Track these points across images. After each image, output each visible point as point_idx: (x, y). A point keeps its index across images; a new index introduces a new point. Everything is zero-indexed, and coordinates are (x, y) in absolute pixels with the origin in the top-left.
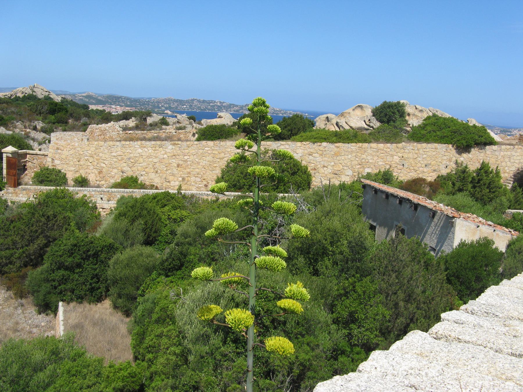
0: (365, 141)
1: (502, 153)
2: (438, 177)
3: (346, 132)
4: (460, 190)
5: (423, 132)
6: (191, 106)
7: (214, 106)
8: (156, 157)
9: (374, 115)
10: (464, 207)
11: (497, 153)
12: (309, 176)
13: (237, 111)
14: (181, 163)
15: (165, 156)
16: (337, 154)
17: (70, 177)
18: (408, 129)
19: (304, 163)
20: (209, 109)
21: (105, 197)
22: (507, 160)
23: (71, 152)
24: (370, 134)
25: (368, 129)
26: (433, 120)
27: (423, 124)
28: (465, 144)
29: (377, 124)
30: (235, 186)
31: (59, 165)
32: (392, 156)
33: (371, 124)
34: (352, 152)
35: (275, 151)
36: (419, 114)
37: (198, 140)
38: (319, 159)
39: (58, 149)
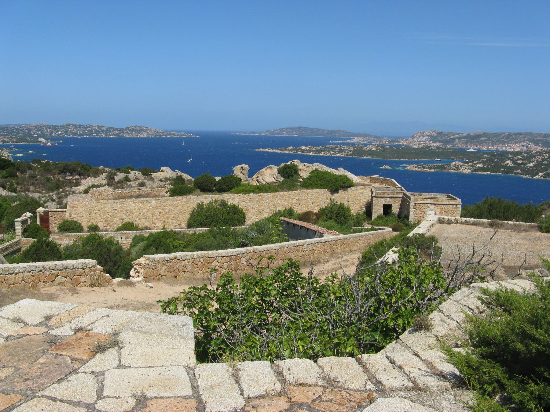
0: (276, 191)
1: (358, 192)
2: (320, 209)
3: (264, 186)
4: (330, 218)
5: (310, 182)
6: (66, 132)
7: (92, 131)
8: (145, 209)
9: (279, 173)
10: (331, 227)
11: (355, 192)
12: (244, 214)
13: (117, 135)
14: (162, 211)
15: (151, 207)
16: (260, 200)
17: (85, 225)
18: (301, 180)
19: (240, 207)
20: (87, 135)
21: (124, 237)
22: (361, 195)
23: (84, 208)
24: (278, 186)
25: (276, 183)
26: (315, 173)
27: (309, 176)
28: (335, 188)
29: (281, 179)
30: (201, 224)
31: (75, 217)
32: (292, 199)
33: (278, 179)
34: (269, 198)
35: (222, 200)
36: (307, 169)
37: (171, 195)
38: (249, 204)
39: (73, 207)
